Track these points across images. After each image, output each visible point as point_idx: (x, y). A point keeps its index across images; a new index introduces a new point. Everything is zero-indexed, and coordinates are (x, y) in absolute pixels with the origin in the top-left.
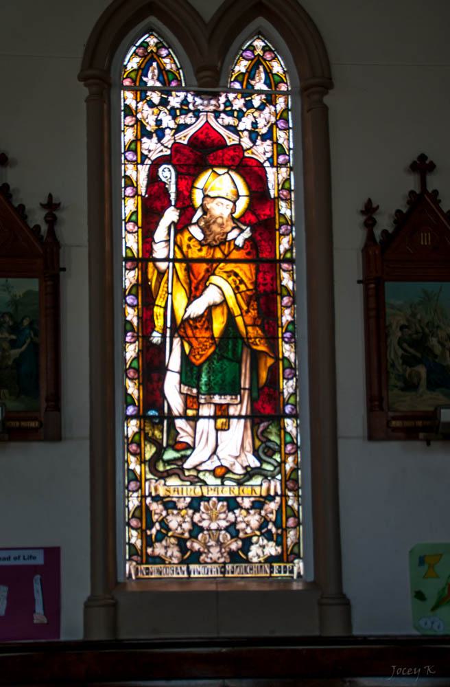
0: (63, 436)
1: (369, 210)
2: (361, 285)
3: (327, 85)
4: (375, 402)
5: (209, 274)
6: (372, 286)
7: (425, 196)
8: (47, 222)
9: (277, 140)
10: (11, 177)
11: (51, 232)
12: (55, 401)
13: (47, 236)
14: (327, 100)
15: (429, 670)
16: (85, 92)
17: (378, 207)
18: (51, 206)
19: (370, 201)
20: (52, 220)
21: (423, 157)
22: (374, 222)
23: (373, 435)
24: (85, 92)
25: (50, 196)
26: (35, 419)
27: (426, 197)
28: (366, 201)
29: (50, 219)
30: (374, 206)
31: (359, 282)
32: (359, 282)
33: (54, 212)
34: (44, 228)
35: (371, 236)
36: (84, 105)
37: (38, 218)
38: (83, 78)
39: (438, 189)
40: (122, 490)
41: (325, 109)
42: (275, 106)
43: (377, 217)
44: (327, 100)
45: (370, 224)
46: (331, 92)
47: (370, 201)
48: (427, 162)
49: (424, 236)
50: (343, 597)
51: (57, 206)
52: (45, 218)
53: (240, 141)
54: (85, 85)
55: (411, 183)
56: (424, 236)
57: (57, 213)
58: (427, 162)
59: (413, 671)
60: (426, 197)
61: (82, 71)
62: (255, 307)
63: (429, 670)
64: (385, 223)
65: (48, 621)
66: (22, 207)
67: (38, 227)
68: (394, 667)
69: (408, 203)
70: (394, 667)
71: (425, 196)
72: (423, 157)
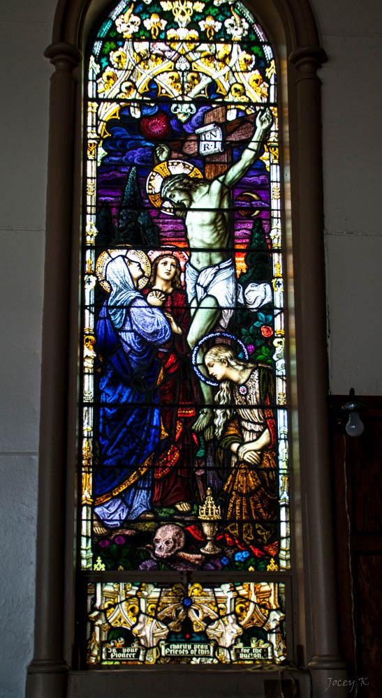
2: (348, 394)
3: (319, 57)
14: (321, 74)
15: (363, 682)
31: (352, 391)
32: (352, 391)
36: (49, 81)
38: (50, 53)
40: (271, 39)
41: (318, 84)
44: (321, 74)
46: (325, 65)
49: (109, 501)
53: (104, 122)
54: (53, 62)
56: (109, 501)
61: (53, 44)
62: (88, 238)
63: (363, 682)
68: (244, 518)
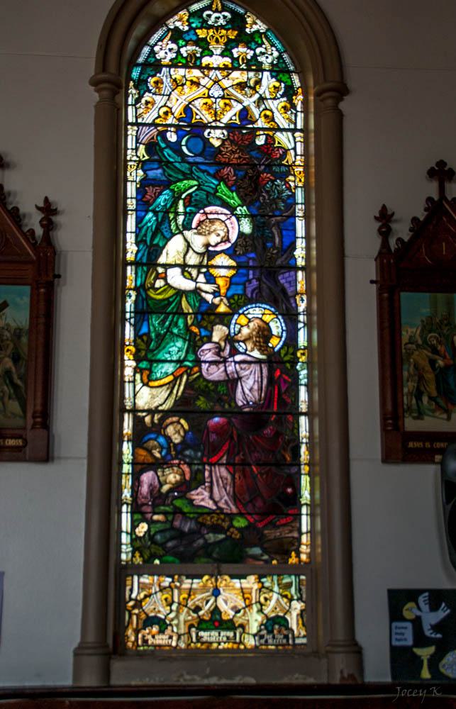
0: (56, 454)
1: (385, 217)
3: (341, 91)
4: (391, 418)
5: (184, 337)
6: (386, 295)
7: (444, 202)
8: (42, 226)
9: (177, 378)
10: (13, 181)
11: (47, 238)
12: (44, 418)
13: (42, 241)
14: (342, 106)
16: (96, 97)
17: (393, 214)
18: (48, 210)
19: (384, 207)
20: (49, 225)
21: (441, 164)
22: (389, 230)
23: (389, 456)
24: (96, 97)
25: (46, 199)
26: (20, 437)
27: (446, 205)
28: (380, 209)
29: (45, 223)
30: (389, 213)
33: (51, 217)
34: (39, 232)
35: (385, 244)
37: (34, 222)
38: (95, 83)
39: (428, 196)
41: (340, 115)
42: (229, 327)
43: (394, 226)
44: (342, 106)
45: (385, 232)
47: (384, 207)
48: (446, 169)
50: (356, 644)
51: (55, 212)
52: (40, 222)
54: (96, 91)
55: (432, 190)
57: (54, 218)
58: (446, 169)
59: (418, 693)
60: (446, 205)
64: (402, 231)
65: (253, 229)
66: (16, 209)
67: (32, 232)
69: (426, 210)
70: (399, 688)
71: (444, 202)
72: (441, 164)
